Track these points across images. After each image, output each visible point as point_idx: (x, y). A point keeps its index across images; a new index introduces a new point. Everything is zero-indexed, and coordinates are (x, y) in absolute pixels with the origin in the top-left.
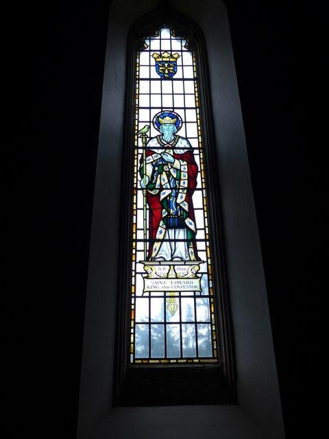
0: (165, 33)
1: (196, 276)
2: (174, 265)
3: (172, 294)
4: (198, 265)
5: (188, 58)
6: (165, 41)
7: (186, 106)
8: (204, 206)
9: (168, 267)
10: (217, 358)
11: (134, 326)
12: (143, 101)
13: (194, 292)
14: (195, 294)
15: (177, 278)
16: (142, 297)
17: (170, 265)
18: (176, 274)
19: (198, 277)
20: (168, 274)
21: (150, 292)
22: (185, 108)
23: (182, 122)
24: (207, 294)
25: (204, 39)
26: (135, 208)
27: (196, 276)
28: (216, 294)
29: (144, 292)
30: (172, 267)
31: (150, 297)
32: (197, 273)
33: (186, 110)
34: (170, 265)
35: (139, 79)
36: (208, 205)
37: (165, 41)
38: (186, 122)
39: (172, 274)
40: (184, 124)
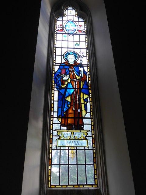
1: (86, 138)
2: (74, 132)
3: (73, 148)
4: (87, 132)
6: (70, 13)
9: (71, 133)
11: (52, 137)
12: (58, 44)
13: (85, 147)
14: (85, 148)
15: (75, 139)
17: (71, 132)
18: (75, 137)
19: (87, 139)
20: (70, 137)
21: (60, 147)
23: (63, 56)
25: (90, 13)
29: (57, 147)
30: (72, 133)
31: (60, 149)
32: (86, 136)
33: (81, 50)
34: (71, 132)
37: (70, 13)
38: (62, 55)
39: (72, 137)
40: (63, 55)
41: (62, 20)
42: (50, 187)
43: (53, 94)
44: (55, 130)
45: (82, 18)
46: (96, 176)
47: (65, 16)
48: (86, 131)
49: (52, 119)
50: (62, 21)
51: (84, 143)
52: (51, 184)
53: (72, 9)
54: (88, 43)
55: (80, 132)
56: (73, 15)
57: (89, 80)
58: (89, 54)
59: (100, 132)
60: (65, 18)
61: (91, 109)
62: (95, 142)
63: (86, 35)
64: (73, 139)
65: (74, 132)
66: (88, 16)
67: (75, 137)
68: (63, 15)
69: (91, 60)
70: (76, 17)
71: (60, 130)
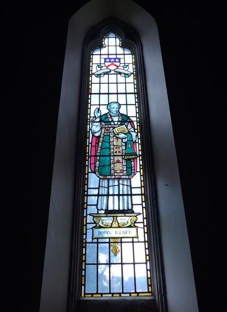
4: (136, 216)
5: (129, 59)
6: (112, 44)
7: (125, 95)
8: (142, 202)
10: (151, 292)
11: (87, 207)
13: (133, 238)
15: (119, 227)
16: (92, 243)
17: (113, 217)
21: (98, 239)
25: (141, 41)
28: (139, 96)
31: (98, 243)
32: (135, 222)
34: (113, 217)
35: (91, 94)
36: (137, 71)
37: (112, 44)
41: (99, 53)
42: (84, 296)
43: (84, 255)
44: (90, 214)
45: (129, 48)
46: (150, 288)
47: (105, 47)
48: (135, 215)
50: (100, 55)
52: (86, 292)
53: (114, 36)
54: (139, 107)
55: (125, 216)
56: (116, 46)
57: (141, 164)
60: (104, 51)
62: (151, 283)
63: (137, 93)
65: (117, 217)
66: (137, 45)
68: (101, 46)
69: (155, 275)
70: (120, 47)
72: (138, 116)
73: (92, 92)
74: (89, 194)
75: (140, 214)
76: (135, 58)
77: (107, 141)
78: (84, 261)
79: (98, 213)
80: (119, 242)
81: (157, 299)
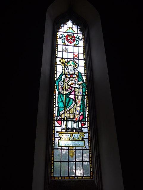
0: (70, 24)
9: (70, 134)
13: (82, 147)
15: (74, 140)
17: (71, 134)
18: (74, 138)
19: (84, 140)
20: (70, 138)
22: (78, 34)
24: (88, 148)
26: (54, 126)
27: (83, 139)
30: (72, 135)
32: (83, 138)
33: (79, 60)
34: (71, 134)
44: (57, 132)
46: (91, 159)
48: (84, 133)
49: (57, 46)
51: (81, 143)
57: (88, 114)
58: (87, 70)
59: (96, 141)
61: (90, 151)
62: (90, 146)
64: (72, 140)
65: (73, 134)
67: (74, 138)
71: (62, 131)
72: (89, 132)
73: (58, 57)
74: (55, 148)
75: (86, 133)
76: (84, 37)
77: (70, 150)
78: (58, 178)
79: (62, 131)
80: (75, 160)
81: (96, 182)
